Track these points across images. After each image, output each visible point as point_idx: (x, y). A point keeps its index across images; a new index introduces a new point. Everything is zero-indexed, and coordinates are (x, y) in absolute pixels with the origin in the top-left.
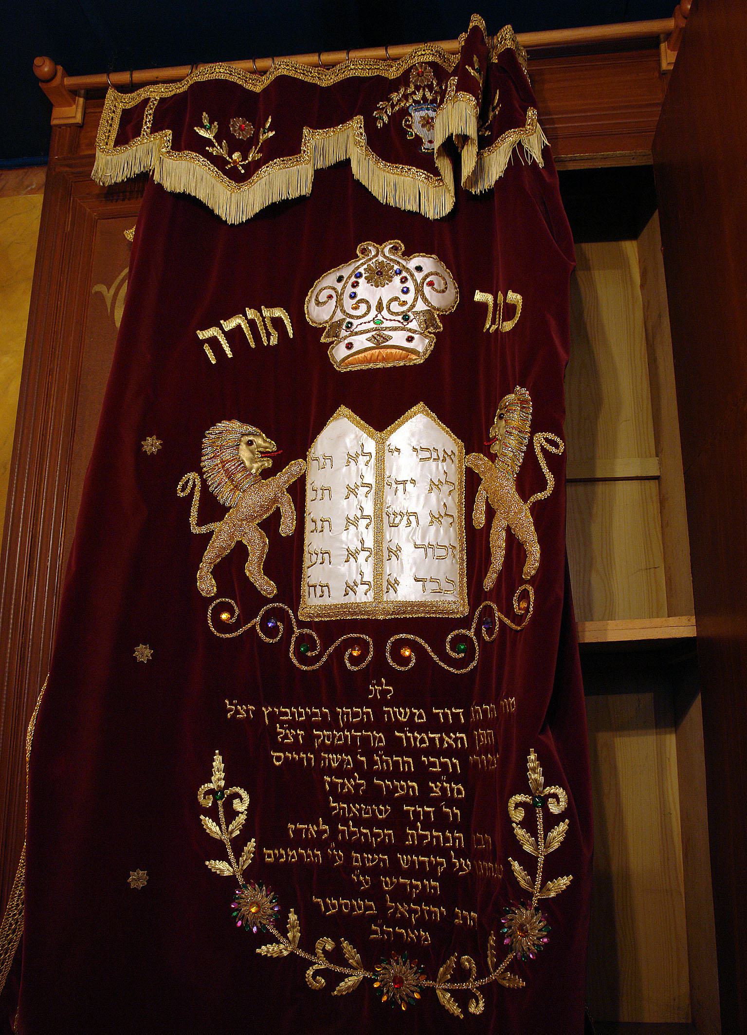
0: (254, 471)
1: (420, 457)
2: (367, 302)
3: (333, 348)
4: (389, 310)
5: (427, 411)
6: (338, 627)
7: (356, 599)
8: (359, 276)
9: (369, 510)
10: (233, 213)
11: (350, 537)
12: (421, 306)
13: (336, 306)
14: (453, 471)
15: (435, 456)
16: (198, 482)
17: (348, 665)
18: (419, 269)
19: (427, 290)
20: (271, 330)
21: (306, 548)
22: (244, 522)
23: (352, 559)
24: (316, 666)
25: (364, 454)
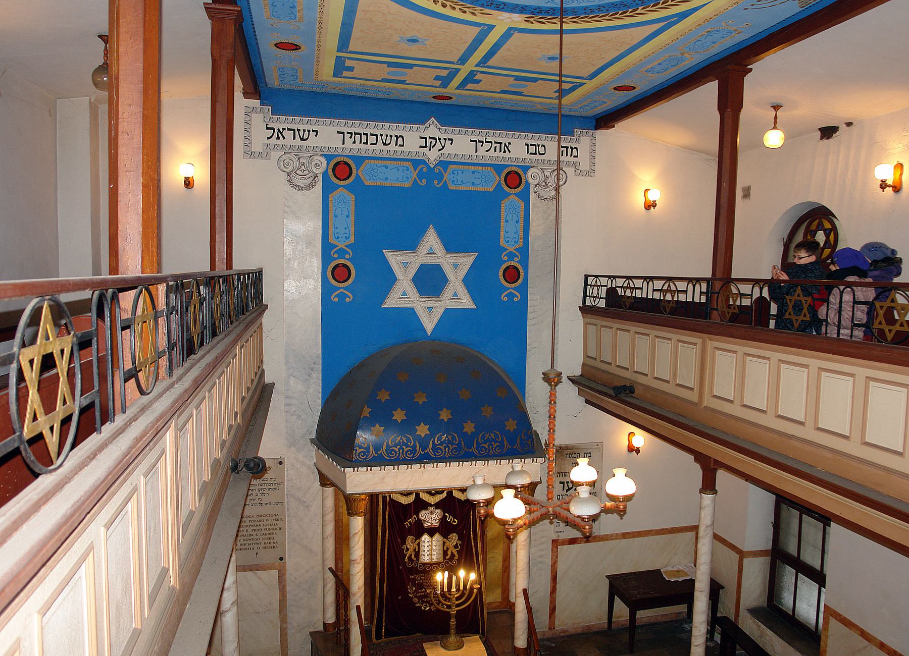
6: (424, 564)
14: (441, 543)
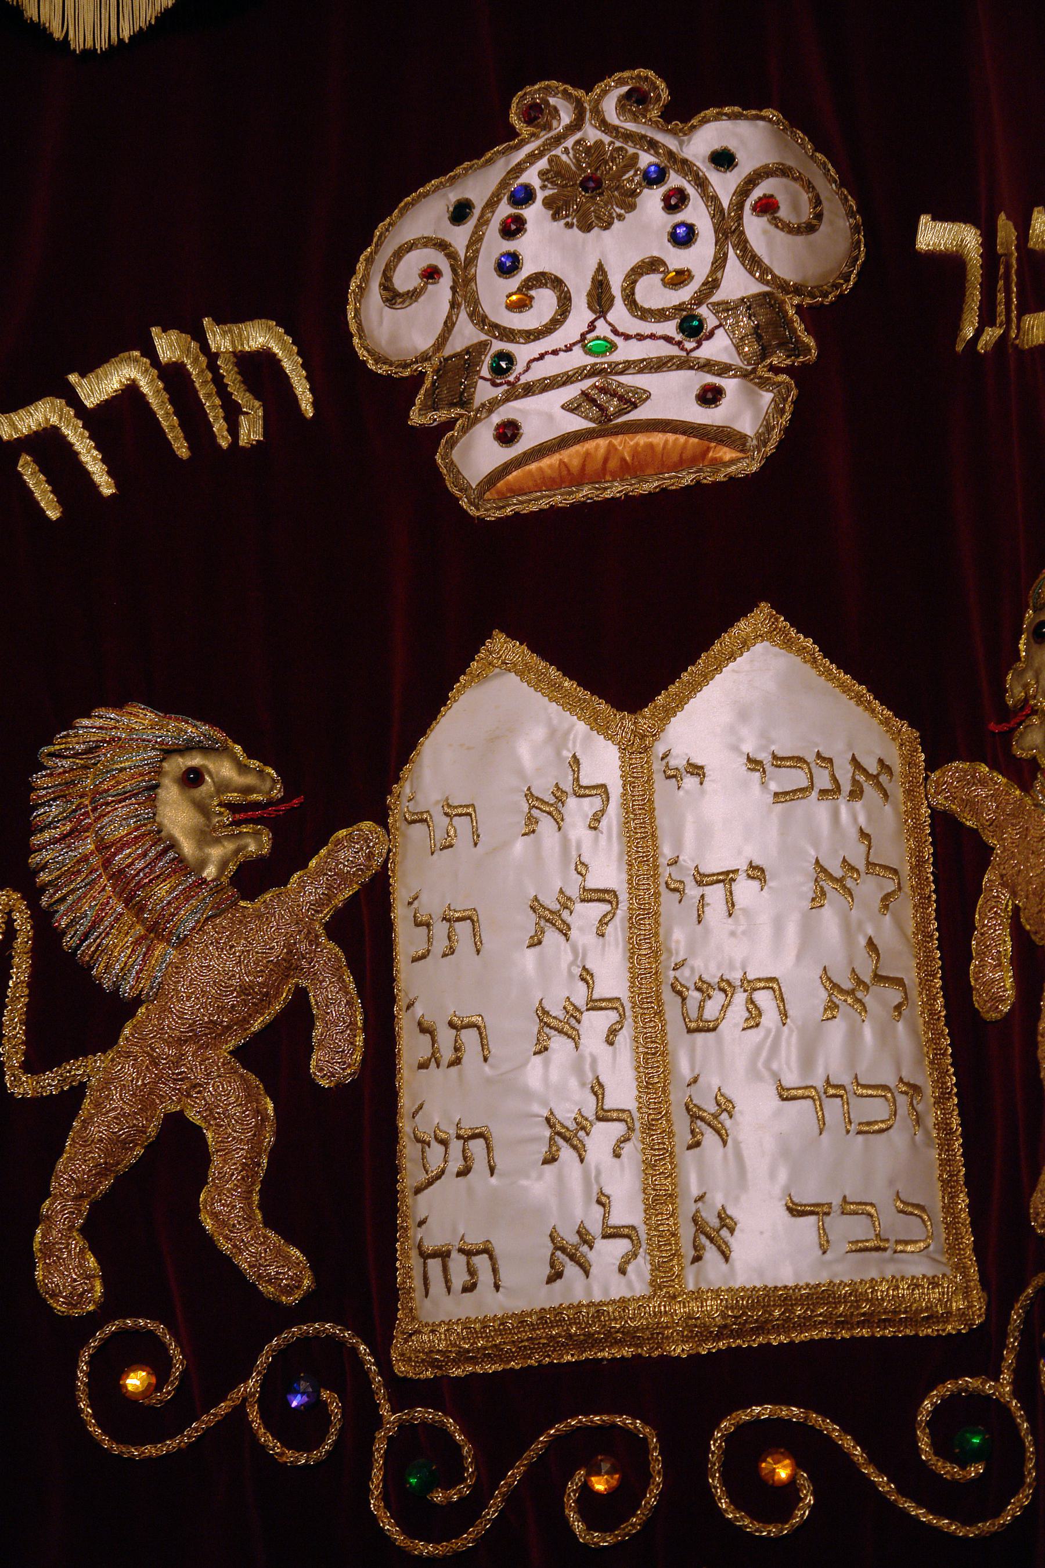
0: (210, 872)
1: (774, 787)
2: (556, 283)
3: (452, 443)
4: (631, 303)
5: (783, 631)
7: (588, 1290)
8: (525, 196)
9: (613, 978)
10: (88, 16)
11: (554, 1076)
12: (738, 283)
13: (454, 305)
14: (882, 827)
15: (823, 780)
16: (22, 921)
17: (578, 1526)
18: (723, 159)
19: (754, 227)
20: (241, 396)
21: (405, 1125)
22: (189, 1049)
23: (567, 1153)
24: (467, 1540)
25: (582, 792)
